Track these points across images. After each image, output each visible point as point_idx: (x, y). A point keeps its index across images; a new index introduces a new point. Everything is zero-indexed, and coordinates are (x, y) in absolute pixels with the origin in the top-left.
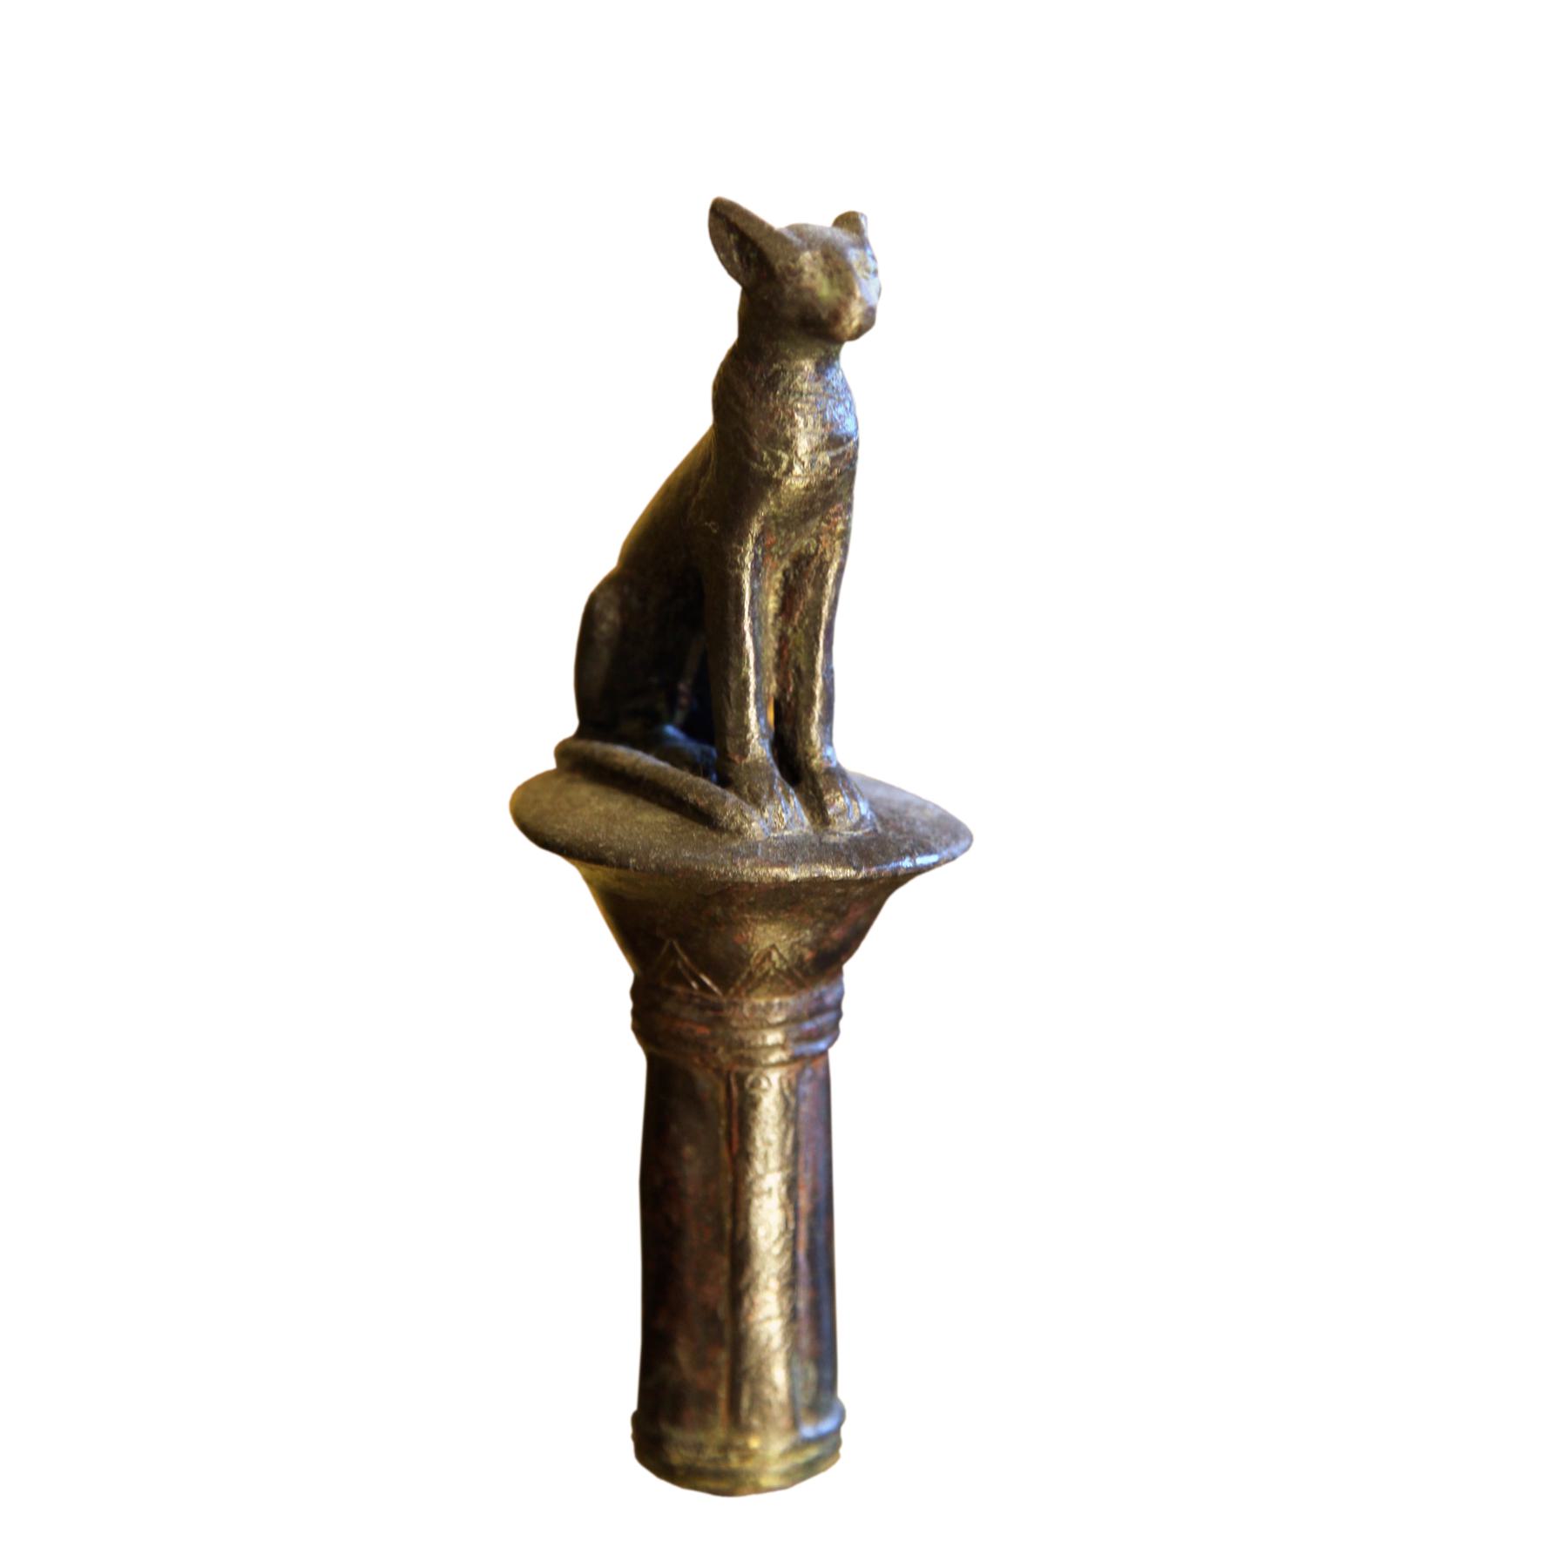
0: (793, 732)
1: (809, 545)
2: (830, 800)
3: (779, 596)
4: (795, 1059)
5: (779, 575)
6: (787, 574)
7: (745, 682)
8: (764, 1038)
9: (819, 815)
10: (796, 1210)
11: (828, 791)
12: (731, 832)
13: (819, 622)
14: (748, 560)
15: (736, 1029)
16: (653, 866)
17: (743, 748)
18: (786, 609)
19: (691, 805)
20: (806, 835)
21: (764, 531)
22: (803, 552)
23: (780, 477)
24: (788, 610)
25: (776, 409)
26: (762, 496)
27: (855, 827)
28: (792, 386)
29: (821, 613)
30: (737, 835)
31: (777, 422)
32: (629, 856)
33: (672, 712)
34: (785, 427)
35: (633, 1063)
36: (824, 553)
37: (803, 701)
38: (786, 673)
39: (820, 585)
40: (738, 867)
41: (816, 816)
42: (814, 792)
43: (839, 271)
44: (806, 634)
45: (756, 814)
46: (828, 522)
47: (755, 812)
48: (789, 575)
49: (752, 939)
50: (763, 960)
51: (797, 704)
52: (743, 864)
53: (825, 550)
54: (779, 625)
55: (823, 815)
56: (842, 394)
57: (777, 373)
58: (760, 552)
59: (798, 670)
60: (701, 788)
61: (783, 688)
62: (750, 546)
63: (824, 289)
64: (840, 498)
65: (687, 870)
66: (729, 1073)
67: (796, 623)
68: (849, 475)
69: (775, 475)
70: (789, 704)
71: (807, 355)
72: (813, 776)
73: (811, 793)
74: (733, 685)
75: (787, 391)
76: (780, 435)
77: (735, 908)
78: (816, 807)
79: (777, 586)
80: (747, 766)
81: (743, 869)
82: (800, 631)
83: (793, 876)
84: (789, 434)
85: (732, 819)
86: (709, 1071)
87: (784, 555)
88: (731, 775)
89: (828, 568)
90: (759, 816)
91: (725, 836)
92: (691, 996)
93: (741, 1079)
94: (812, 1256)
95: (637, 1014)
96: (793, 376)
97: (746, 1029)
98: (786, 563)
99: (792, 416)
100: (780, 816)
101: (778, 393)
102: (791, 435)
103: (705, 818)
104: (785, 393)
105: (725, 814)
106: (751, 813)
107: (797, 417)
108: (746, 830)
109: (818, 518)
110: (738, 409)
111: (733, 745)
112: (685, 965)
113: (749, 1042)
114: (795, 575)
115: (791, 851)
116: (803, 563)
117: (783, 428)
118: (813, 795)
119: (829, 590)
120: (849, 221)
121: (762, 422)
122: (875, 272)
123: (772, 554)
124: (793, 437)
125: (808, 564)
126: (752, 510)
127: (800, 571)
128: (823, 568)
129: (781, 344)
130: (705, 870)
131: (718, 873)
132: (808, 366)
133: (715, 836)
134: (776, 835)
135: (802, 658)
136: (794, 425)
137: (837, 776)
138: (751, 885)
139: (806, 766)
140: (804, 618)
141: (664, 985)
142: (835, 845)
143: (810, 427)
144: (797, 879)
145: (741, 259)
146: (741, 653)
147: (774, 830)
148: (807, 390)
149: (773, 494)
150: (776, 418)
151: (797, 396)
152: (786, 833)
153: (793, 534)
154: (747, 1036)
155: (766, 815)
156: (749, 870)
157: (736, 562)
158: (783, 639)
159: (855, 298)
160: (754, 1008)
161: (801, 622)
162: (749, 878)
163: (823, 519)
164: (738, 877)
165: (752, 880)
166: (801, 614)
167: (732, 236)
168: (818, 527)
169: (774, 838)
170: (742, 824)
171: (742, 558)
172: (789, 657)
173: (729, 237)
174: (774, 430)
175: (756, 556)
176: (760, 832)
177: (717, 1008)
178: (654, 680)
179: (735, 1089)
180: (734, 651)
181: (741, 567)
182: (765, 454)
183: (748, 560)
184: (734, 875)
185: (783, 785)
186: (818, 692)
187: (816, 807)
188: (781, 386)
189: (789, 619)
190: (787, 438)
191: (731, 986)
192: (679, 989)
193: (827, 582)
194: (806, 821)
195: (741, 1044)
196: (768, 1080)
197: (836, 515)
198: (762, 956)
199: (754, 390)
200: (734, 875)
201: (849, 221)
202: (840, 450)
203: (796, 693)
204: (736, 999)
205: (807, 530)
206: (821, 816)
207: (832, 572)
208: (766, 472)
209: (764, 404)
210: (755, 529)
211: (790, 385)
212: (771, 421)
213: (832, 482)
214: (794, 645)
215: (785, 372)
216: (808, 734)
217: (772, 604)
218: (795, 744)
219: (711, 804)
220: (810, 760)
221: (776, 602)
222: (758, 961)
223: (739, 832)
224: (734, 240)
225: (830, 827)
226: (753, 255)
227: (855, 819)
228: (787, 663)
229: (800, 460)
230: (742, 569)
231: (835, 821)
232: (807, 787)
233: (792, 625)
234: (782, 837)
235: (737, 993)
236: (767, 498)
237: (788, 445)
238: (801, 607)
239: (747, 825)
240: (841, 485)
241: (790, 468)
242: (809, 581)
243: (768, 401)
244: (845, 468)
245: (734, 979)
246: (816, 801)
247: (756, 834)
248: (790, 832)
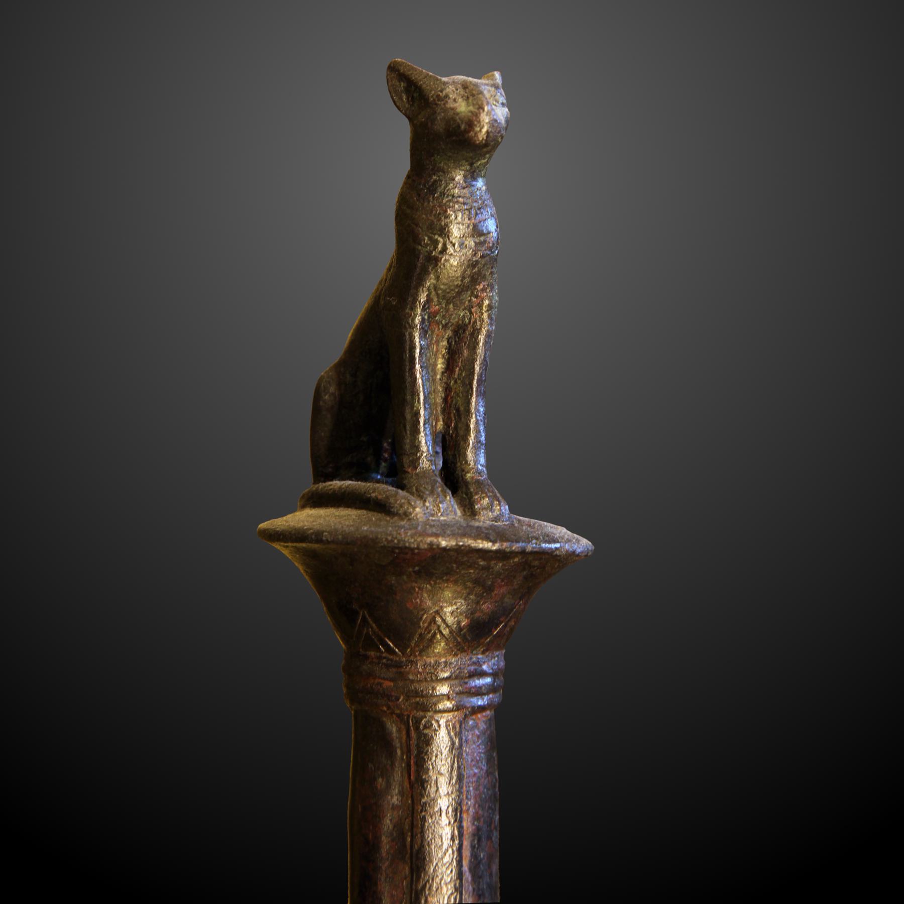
0: (454, 456)
1: (464, 316)
2: (477, 499)
3: (445, 359)
4: (457, 708)
5: (445, 343)
6: (450, 341)
7: (417, 414)
8: (434, 689)
9: (469, 509)
10: (460, 828)
11: (476, 493)
12: (400, 514)
13: (473, 373)
14: (418, 320)
15: (412, 681)
16: (340, 537)
17: (415, 463)
18: (449, 368)
19: (373, 499)
20: (457, 521)
22: (460, 322)
23: (437, 255)
24: (451, 367)
25: (434, 206)
26: (425, 272)
27: (496, 519)
28: (446, 191)
29: (474, 368)
30: (404, 517)
31: (435, 215)
32: (323, 532)
33: (378, 465)
34: (441, 218)
36: (475, 322)
37: (461, 433)
38: (449, 413)
40: (401, 535)
41: (467, 510)
42: (467, 495)
43: (473, 95)
44: (464, 383)
45: (419, 503)
46: (476, 297)
47: (418, 502)
48: (452, 342)
49: (421, 605)
50: (430, 624)
51: (457, 435)
52: (406, 533)
53: (476, 319)
54: (445, 379)
55: (472, 509)
57: (435, 181)
58: (426, 317)
59: (458, 410)
60: (380, 489)
61: (447, 424)
62: (419, 311)
63: (462, 107)
65: (365, 537)
66: (408, 716)
67: (456, 376)
69: (434, 253)
70: (452, 436)
71: (458, 166)
72: (466, 484)
73: (464, 496)
74: (408, 416)
75: (443, 194)
76: (437, 224)
77: (405, 577)
79: (444, 351)
80: (417, 475)
81: (405, 537)
82: (459, 382)
84: (443, 223)
85: (401, 506)
86: (394, 716)
87: (447, 324)
88: (405, 482)
89: (478, 333)
90: (422, 505)
91: (396, 518)
92: (380, 658)
93: (418, 721)
96: (447, 184)
97: (420, 681)
98: (449, 333)
99: (446, 211)
100: (438, 506)
101: (436, 195)
103: (381, 507)
104: (441, 196)
105: (396, 502)
108: (411, 514)
109: (469, 293)
110: (408, 211)
111: (408, 461)
112: (374, 632)
113: (422, 691)
114: (455, 341)
115: (444, 529)
116: (461, 331)
117: (440, 220)
118: (466, 497)
121: (424, 216)
123: (438, 323)
124: (447, 225)
125: (464, 331)
126: (420, 282)
127: (458, 338)
129: (437, 158)
130: (377, 538)
131: (386, 539)
132: (459, 178)
133: (388, 518)
134: (434, 518)
135: (460, 402)
136: (448, 217)
138: (412, 550)
139: (463, 479)
140: (462, 372)
141: (362, 652)
142: (478, 527)
143: (459, 218)
144: (447, 546)
145: (408, 99)
147: (433, 515)
148: (458, 193)
149: (433, 268)
150: (434, 212)
151: (450, 198)
152: (442, 518)
153: (451, 306)
154: (421, 687)
155: (427, 504)
156: (410, 538)
157: (409, 323)
158: (447, 389)
159: (484, 110)
160: (425, 665)
161: (460, 375)
162: (410, 543)
163: (472, 294)
164: (402, 542)
165: (412, 546)
166: (460, 369)
167: (402, 85)
168: (469, 301)
169: (432, 520)
170: (408, 509)
171: (413, 320)
172: (452, 401)
173: (400, 85)
174: (433, 222)
175: (423, 319)
176: (421, 515)
177: (398, 665)
178: (364, 439)
179: (413, 734)
181: (412, 327)
182: (426, 238)
183: (418, 320)
184: (399, 541)
185: (442, 487)
186: (472, 426)
188: (439, 190)
189: (452, 373)
190: (442, 226)
191: (408, 646)
192: (372, 653)
193: (478, 344)
194: (459, 513)
195: (417, 694)
196: (438, 722)
197: (483, 290)
198: (429, 620)
199: (419, 195)
200: (399, 541)
203: (456, 428)
204: (412, 658)
205: (462, 303)
206: (470, 510)
209: (426, 204)
210: (423, 298)
211: (444, 191)
213: (477, 261)
214: (455, 392)
215: (441, 181)
216: (465, 456)
218: (455, 464)
219: (387, 497)
220: (465, 475)
221: (443, 363)
222: (426, 625)
223: (406, 514)
224: (404, 87)
225: (477, 517)
226: (415, 95)
227: (496, 513)
228: (451, 407)
229: (451, 242)
230: (413, 328)
231: (480, 513)
232: (462, 492)
233: (453, 378)
234: (439, 521)
235: (413, 653)
237: (444, 231)
238: (460, 364)
239: (411, 510)
242: (465, 344)
243: (429, 201)
244: (486, 252)
245: (410, 640)
246: (468, 500)
247: (418, 516)
248: (445, 518)
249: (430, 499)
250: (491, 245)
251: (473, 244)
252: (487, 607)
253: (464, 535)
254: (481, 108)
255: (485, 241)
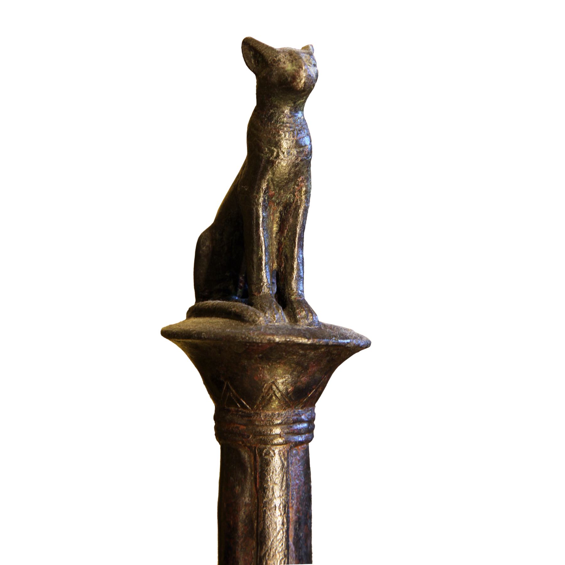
1: (290, 198)
2: (298, 312)
3: (278, 224)
4: (286, 443)
5: (278, 214)
6: (281, 213)
7: (261, 259)
8: (271, 430)
9: (293, 318)
10: (288, 517)
11: (298, 308)
12: (250, 321)
13: (296, 233)
14: (261, 200)
15: (258, 426)
16: (213, 336)
17: (259, 289)
18: (281, 230)
19: (233, 312)
20: (286, 326)
21: (268, 188)
22: (288, 201)
23: (273, 159)
24: (282, 230)
25: (271, 129)
26: (265, 170)
27: (310, 324)
28: (279, 119)
29: (296, 230)
30: (252, 323)
31: (272, 134)
32: (202, 332)
33: (236, 290)
34: (275, 136)
35: (216, 448)
36: (297, 201)
37: (288, 270)
38: (281, 258)
39: (296, 217)
40: (251, 335)
41: (292, 319)
42: (292, 309)
43: (296, 60)
44: (290, 240)
45: (262, 314)
46: (298, 185)
47: (261, 314)
48: (282, 214)
49: (263, 378)
50: (269, 390)
51: (286, 272)
52: (254, 333)
53: (297, 200)
54: (278, 237)
55: (295, 318)
56: (303, 127)
57: (272, 113)
58: (266, 198)
59: (286, 256)
60: (237, 305)
61: (279, 265)
62: (262, 195)
64: (302, 174)
65: (228, 336)
66: (255, 448)
67: (285, 235)
68: (308, 163)
69: (271, 158)
70: (282, 273)
71: (286, 104)
72: (292, 302)
73: (290, 310)
74: (255, 260)
75: (277, 121)
76: (273, 140)
77: (253, 361)
78: (293, 317)
79: (277, 220)
80: (260, 297)
81: (253, 336)
82: (287, 239)
83: (277, 340)
84: (277, 140)
85: (251, 316)
86: (247, 448)
87: (279, 203)
88: (253, 301)
89: (299, 208)
90: (264, 315)
91: (248, 324)
92: (238, 411)
93: (261, 451)
94: (297, 542)
95: (218, 429)
96: (279, 115)
97: (263, 426)
98: (281, 208)
99: (279, 132)
101: (272, 122)
102: (278, 140)
103: (238, 317)
104: (276, 122)
105: (247, 314)
106: (260, 314)
107: (281, 132)
109: (293, 183)
111: (255, 288)
112: (234, 395)
113: (264, 432)
114: (285, 213)
115: (277, 331)
116: (288, 207)
117: (275, 137)
118: (291, 311)
119: (300, 219)
120: (309, 50)
121: (265, 135)
122: (315, 65)
123: (274, 202)
124: (279, 141)
125: (290, 207)
126: (263, 176)
127: (287, 211)
128: (297, 208)
129: (273, 99)
130: (236, 336)
131: (242, 337)
132: (287, 111)
133: (243, 324)
134: (271, 324)
135: (288, 251)
136: (280, 135)
137: (304, 305)
138: (258, 343)
139: (289, 299)
140: (289, 233)
141: (226, 407)
142: (299, 330)
143: (287, 137)
144: (279, 341)
145: (255, 62)
146: (259, 246)
147: (270, 322)
148: (286, 121)
149: (271, 167)
150: (271, 133)
151: (281, 124)
152: (276, 324)
153: (282, 191)
154: (263, 429)
155: (267, 315)
156: (256, 336)
157: (255, 202)
158: (280, 243)
159: (302, 69)
160: (266, 416)
161: (287, 234)
162: (256, 339)
163: (295, 184)
164: (251, 339)
165: (258, 341)
166: (288, 231)
167: (251, 53)
168: (293, 188)
169: (270, 325)
170: (255, 318)
171: (258, 200)
174: (270, 138)
175: (264, 199)
176: (263, 322)
177: (249, 416)
178: (228, 274)
179: (258, 459)
180: (255, 245)
181: (258, 204)
182: (266, 149)
183: (261, 200)
184: (249, 338)
185: (276, 304)
186: (295, 266)
187: (293, 317)
188: (275, 119)
189: (283, 233)
190: (276, 141)
191: (255, 404)
192: (233, 408)
193: (299, 215)
194: (287, 320)
195: (261, 434)
196: (274, 451)
197: (302, 181)
198: (268, 388)
199: (262, 122)
200: (249, 338)
201: (306, 48)
202: (301, 149)
203: (285, 267)
204: (257, 411)
205: (289, 189)
206: (294, 319)
207: (301, 211)
208: (267, 157)
209: (266, 127)
210: (264, 186)
211: (278, 119)
212: (269, 135)
213: (298, 163)
214: (284, 245)
216: (291, 285)
217: (275, 228)
218: (285, 290)
219: (242, 311)
220: (291, 297)
221: (277, 227)
222: (266, 390)
223: (254, 322)
224: (252, 54)
225: (298, 323)
226: (260, 59)
227: (310, 321)
228: (282, 254)
229: (282, 151)
230: (258, 205)
231: (300, 321)
232: (289, 308)
233: (283, 236)
234: (274, 325)
235: (258, 408)
236: (268, 170)
237: (277, 145)
238: (287, 227)
239: (257, 319)
240: (302, 166)
241: (278, 156)
242: (291, 215)
244: (303, 158)
245: (256, 400)
246: (292, 313)
247: (261, 323)
248: (278, 324)
249: (269, 312)
250: (307, 153)
251: (295, 152)
252: (304, 379)
253: (290, 334)
254: (301, 67)
255: (303, 151)
